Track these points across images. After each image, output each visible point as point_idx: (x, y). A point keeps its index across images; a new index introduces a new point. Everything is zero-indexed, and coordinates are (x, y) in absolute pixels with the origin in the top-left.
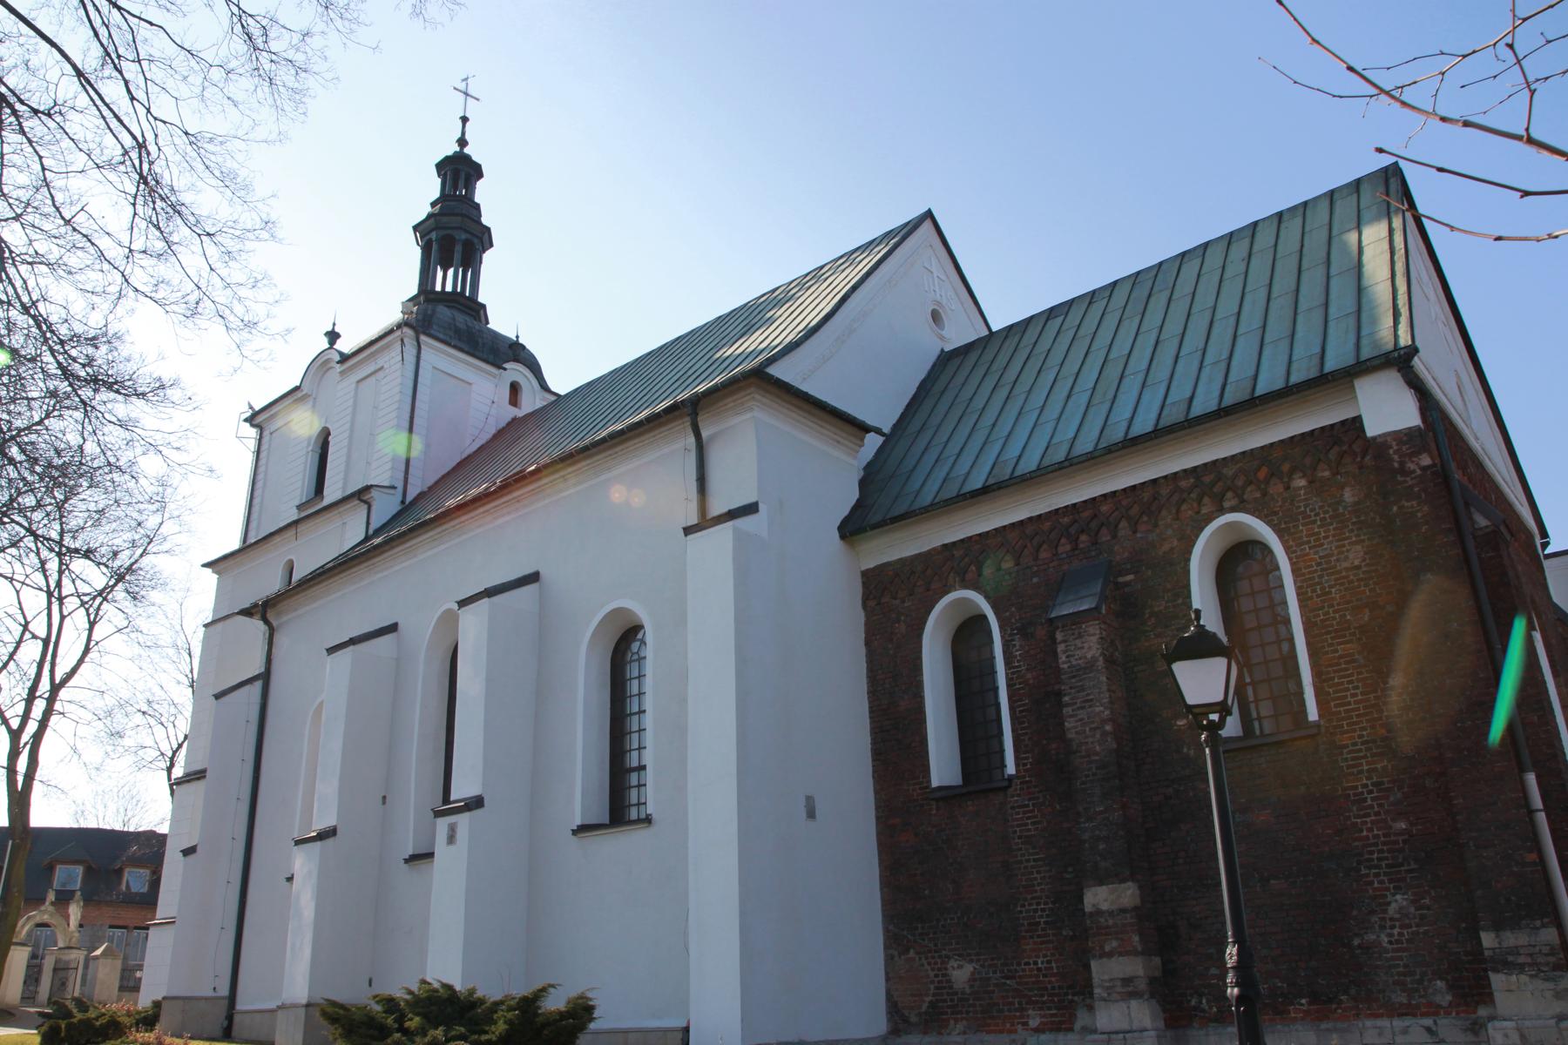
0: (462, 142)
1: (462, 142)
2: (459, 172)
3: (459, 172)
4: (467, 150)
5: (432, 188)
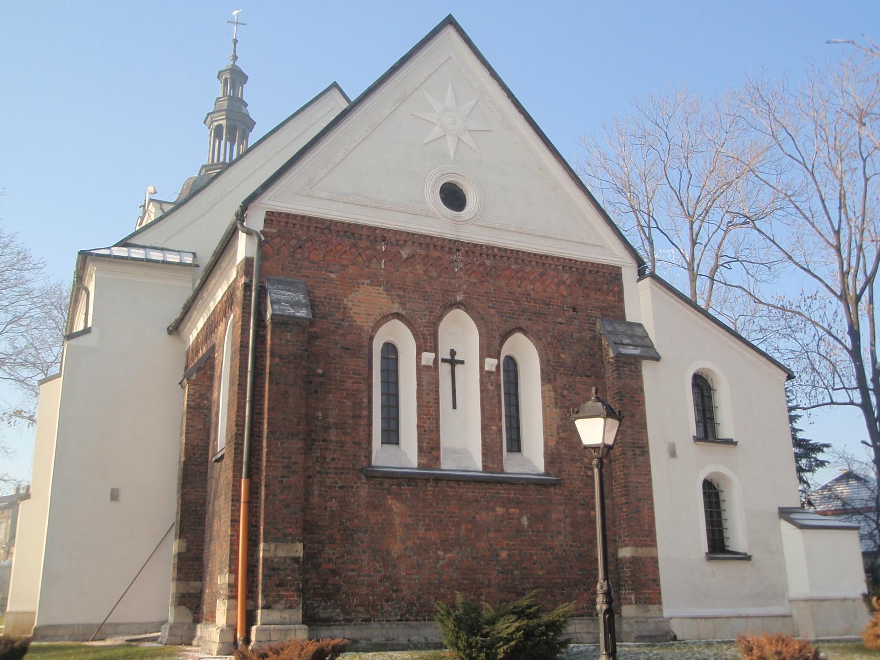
0: (235, 58)
1: (235, 58)
2: (235, 78)
3: (235, 78)
4: (236, 63)
5: (218, 90)
